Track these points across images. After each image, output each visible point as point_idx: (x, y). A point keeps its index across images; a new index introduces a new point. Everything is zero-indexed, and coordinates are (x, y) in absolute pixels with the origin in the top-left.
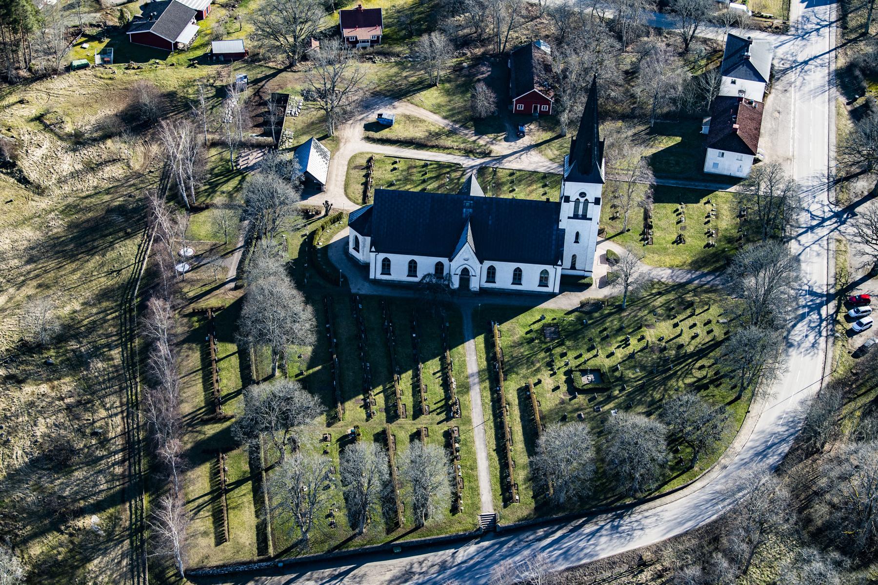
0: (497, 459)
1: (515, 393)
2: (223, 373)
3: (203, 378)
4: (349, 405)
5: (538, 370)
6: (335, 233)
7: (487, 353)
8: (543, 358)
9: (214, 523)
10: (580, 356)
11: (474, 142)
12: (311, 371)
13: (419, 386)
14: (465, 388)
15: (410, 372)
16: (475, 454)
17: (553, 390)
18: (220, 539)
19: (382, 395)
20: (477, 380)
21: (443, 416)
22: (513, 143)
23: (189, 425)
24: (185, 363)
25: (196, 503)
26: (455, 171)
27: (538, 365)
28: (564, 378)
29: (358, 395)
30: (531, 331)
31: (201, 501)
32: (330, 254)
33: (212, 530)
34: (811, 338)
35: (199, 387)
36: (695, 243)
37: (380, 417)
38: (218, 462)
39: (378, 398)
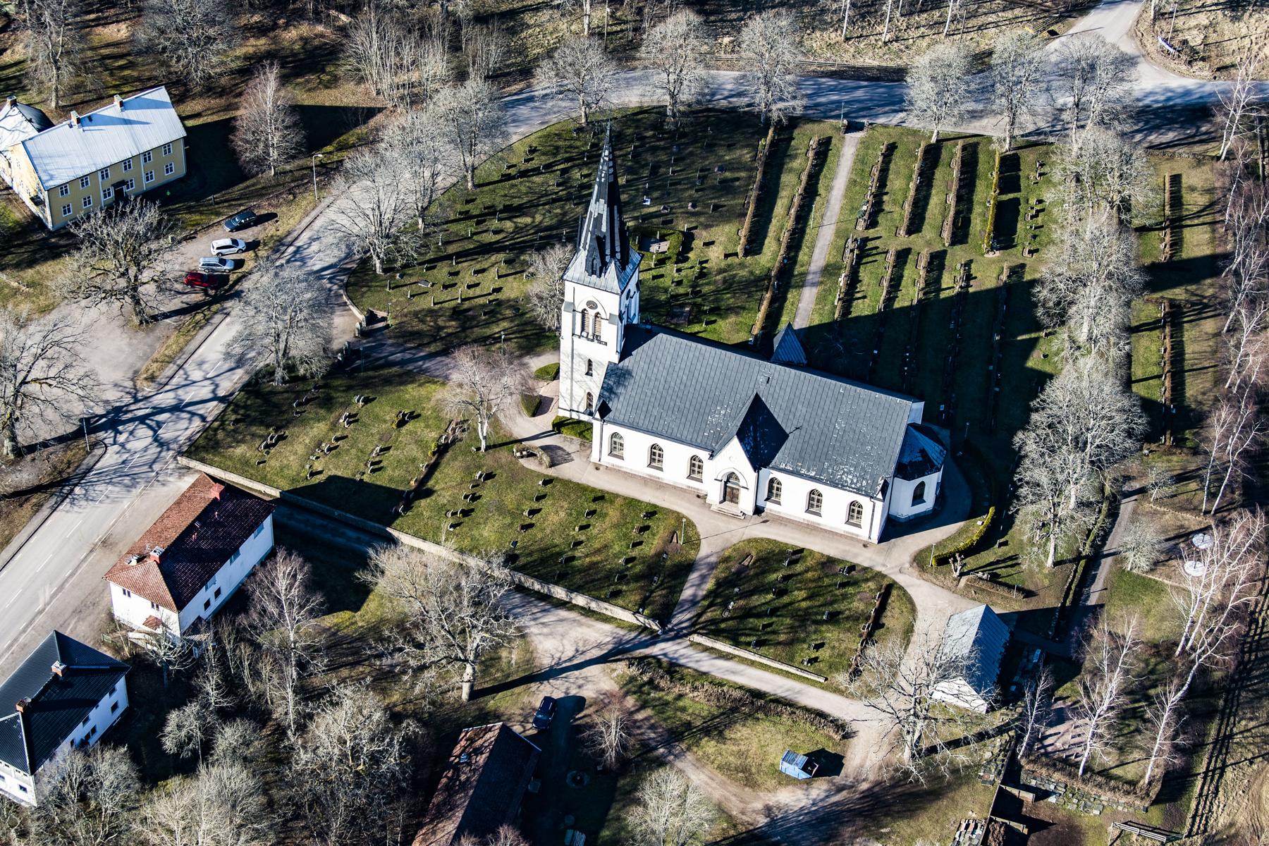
0: (820, 185)
1: (765, 249)
2: (1154, 359)
3: (1183, 360)
4: (990, 283)
5: (720, 271)
6: (951, 539)
7: (781, 308)
8: (707, 284)
9: (1181, 197)
10: (654, 278)
11: (643, 707)
12: (1033, 335)
13: (890, 286)
14: (830, 271)
15: (896, 305)
16: (845, 196)
17: (713, 243)
18: (1176, 180)
19: (944, 286)
20: (810, 277)
21: (870, 245)
22: (573, 692)
23: (1206, 306)
24: (1208, 385)
25: (1201, 220)
26: (713, 621)
27: (719, 277)
28: (691, 255)
29: (975, 293)
30: (708, 323)
31: (1196, 222)
32: (968, 502)
33: (1184, 191)
34: (315, 246)
35: (1189, 349)
36: (385, 411)
37: (957, 256)
38: (1172, 256)
39: (950, 283)
